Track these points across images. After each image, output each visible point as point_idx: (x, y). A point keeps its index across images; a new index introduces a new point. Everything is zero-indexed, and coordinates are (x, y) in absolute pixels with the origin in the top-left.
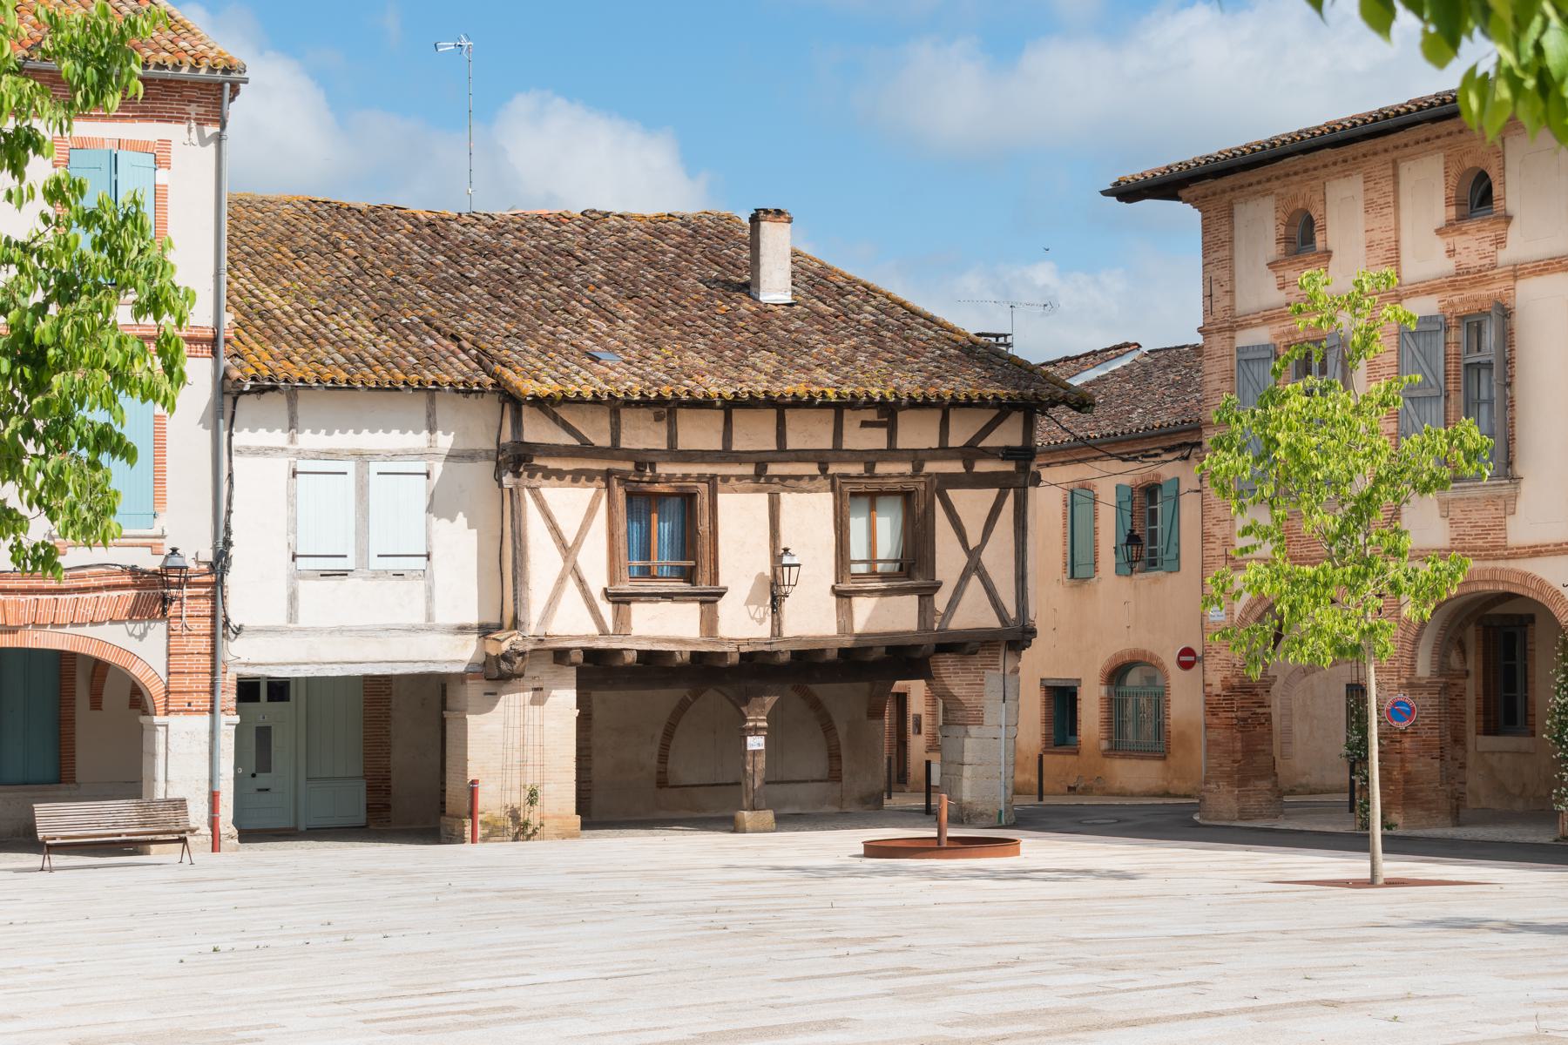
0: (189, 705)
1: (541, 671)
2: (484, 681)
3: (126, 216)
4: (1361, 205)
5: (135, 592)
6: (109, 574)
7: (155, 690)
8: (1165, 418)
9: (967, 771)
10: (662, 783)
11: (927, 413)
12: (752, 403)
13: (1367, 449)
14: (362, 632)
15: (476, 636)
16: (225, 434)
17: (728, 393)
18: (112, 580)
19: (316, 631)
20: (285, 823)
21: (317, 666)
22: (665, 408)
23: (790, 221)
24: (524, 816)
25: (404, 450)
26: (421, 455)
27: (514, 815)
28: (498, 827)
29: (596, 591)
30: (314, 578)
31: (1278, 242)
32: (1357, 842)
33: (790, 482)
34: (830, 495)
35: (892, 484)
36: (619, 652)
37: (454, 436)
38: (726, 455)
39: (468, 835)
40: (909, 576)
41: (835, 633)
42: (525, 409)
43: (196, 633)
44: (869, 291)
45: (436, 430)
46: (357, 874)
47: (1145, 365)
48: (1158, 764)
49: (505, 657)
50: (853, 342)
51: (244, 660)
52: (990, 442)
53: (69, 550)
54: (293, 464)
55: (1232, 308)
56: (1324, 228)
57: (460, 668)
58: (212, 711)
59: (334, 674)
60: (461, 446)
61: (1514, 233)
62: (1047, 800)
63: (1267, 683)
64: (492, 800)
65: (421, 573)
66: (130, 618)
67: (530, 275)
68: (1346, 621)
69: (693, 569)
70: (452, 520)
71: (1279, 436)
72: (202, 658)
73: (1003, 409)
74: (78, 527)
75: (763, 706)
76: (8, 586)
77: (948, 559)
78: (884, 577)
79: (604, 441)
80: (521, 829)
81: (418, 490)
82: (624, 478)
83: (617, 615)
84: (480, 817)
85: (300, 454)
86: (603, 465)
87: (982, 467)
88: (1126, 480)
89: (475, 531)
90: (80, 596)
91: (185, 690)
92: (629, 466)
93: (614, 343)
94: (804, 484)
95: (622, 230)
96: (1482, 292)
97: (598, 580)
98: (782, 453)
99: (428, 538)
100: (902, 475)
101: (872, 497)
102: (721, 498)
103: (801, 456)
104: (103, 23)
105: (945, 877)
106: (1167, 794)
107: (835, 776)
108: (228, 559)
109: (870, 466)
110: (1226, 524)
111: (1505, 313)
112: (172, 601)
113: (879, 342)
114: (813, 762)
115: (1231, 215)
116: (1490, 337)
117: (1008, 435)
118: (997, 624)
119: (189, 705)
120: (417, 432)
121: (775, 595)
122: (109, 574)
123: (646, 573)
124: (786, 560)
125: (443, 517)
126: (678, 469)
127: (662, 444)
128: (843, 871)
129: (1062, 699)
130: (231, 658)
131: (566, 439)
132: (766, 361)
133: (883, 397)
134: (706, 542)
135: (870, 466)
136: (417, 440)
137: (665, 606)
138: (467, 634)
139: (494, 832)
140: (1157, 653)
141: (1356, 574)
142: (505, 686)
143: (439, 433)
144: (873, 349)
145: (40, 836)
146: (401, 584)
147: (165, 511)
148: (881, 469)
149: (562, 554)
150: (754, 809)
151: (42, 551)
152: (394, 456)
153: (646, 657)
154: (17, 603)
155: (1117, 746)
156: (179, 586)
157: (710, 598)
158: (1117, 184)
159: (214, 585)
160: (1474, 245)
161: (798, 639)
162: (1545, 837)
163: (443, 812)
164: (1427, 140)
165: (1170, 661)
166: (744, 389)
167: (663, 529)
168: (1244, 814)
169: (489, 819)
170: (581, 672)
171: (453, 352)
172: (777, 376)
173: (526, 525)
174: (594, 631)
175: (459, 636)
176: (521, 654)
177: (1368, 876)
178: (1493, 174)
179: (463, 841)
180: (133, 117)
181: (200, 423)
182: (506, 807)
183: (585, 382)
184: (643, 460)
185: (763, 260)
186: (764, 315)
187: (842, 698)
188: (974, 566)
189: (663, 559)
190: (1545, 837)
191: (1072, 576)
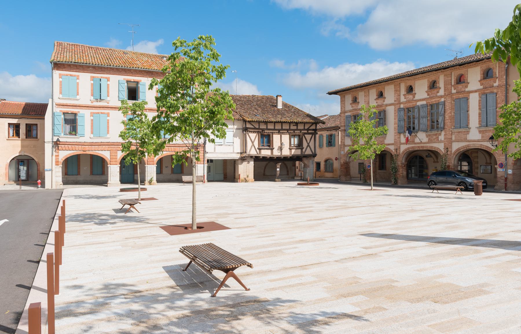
1: (248, 159)
3: (226, 94)
4: (364, 96)
8: (333, 125)
9: (307, 174)
10: (264, 175)
11: (302, 124)
12: (278, 122)
13: (371, 130)
14: (224, 153)
17: (275, 121)
20: (212, 179)
22: (266, 123)
23: (282, 97)
24: (246, 179)
26: (232, 129)
27: (245, 179)
29: (257, 148)
30: (217, 145)
31: (352, 101)
32: (370, 185)
33: (283, 133)
34: (289, 135)
35: (297, 134)
36: (260, 156)
38: (274, 129)
39: (239, 181)
40: (299, 147)
41: (289, 154)
42: (247, 122)
44: (293, 107)
46: (228, 186)
47: (329, 118)
48: (332, 173)
49: (244, 157)
50: (291, 114)
52: (311, 128)
55: (345, 110)
56: (358, 99)
57: (238, 158)
58: (204, 164)
61: (386, 100)
62: (316, 178)
63: (350, 162)
64: (242, 177)
67: (246, 104)
68: (368, 153)
69: (270, 145)
70: (237, 138)
71: (359, 128)
73: (313, 124)
74: (221, 136)
75: (279, 164)
77: (305, 144)
78: (296, 147)
79: (258, 127)
80: (246, 181)
82: (260, 133)
83: (259, 151)
84: (240, 179)
86: (257, 131)
87: (310, 132)
88: (328, 134)
92: (261, 131)
93: (258, 113)
94: (285, 134)
95: (258, 98)
96: (381, 108)
97: (257, 147)
98: (282, 129)
99: (233, 140)
100: (299, 133)
101: (294, 136)
102: (274, 135)
103: (285, 130)
104: (221, 67)
105: (311, 188)
106: (333, 178)
107: (288, 174)
108: (206, 143)
109: (294, 132)
110: (344, 140)
111: (385, 111)
112: (198, 148)
113: (295, 114)
114: (286, 173)
115: (345, 97)
116: (382, 114)
117: (313, 127)
118: (311, 154)
120: (232, 125)
121: (281, 149)
123: (263, 146)
124: (283, 144)
126: (268, 131)
127: (265, 128)
128: (293, 187)
129: (318, 164)
131: (252, 127)
132: (280, 116)
133: (296, 122)
134: (272, 141)
135: (294, 132)
137: (266, 150)
139: (242, 181)
140: (332, 158)
141: (370, 147)
144: (294, 115)
145: (183, 180)
148: (296, 132)
150: (278, 179)
151: (212, 140)
153: (263, 157)
154: (177, 148)
155: (326, 171)
156: (199, 146)
157: (272, 149)
158: (329, 92)
159: (204, 146)
160: (380, 102)
161: (284, 155)
162: (390, 184)
163: (235, 178)
164: (374, 87)
165: (334, 159)
166: (277, 120)
167: (265, 140)
168: (346, 180)
170: (254, 159)
171: (236, 114)
172: (281, 119)
174: (256, 154)
176: (246, 157)
177: (371, 189)
178: (383, 92)
179: (238, 182)
183: (255, 119)
184: (263, 130)
185: (278, 102)
186: (278, 110)
187: (289, 163)
188: (308, 146)
189: (265, 144)
190: (390, 184)
191: (320, 147)
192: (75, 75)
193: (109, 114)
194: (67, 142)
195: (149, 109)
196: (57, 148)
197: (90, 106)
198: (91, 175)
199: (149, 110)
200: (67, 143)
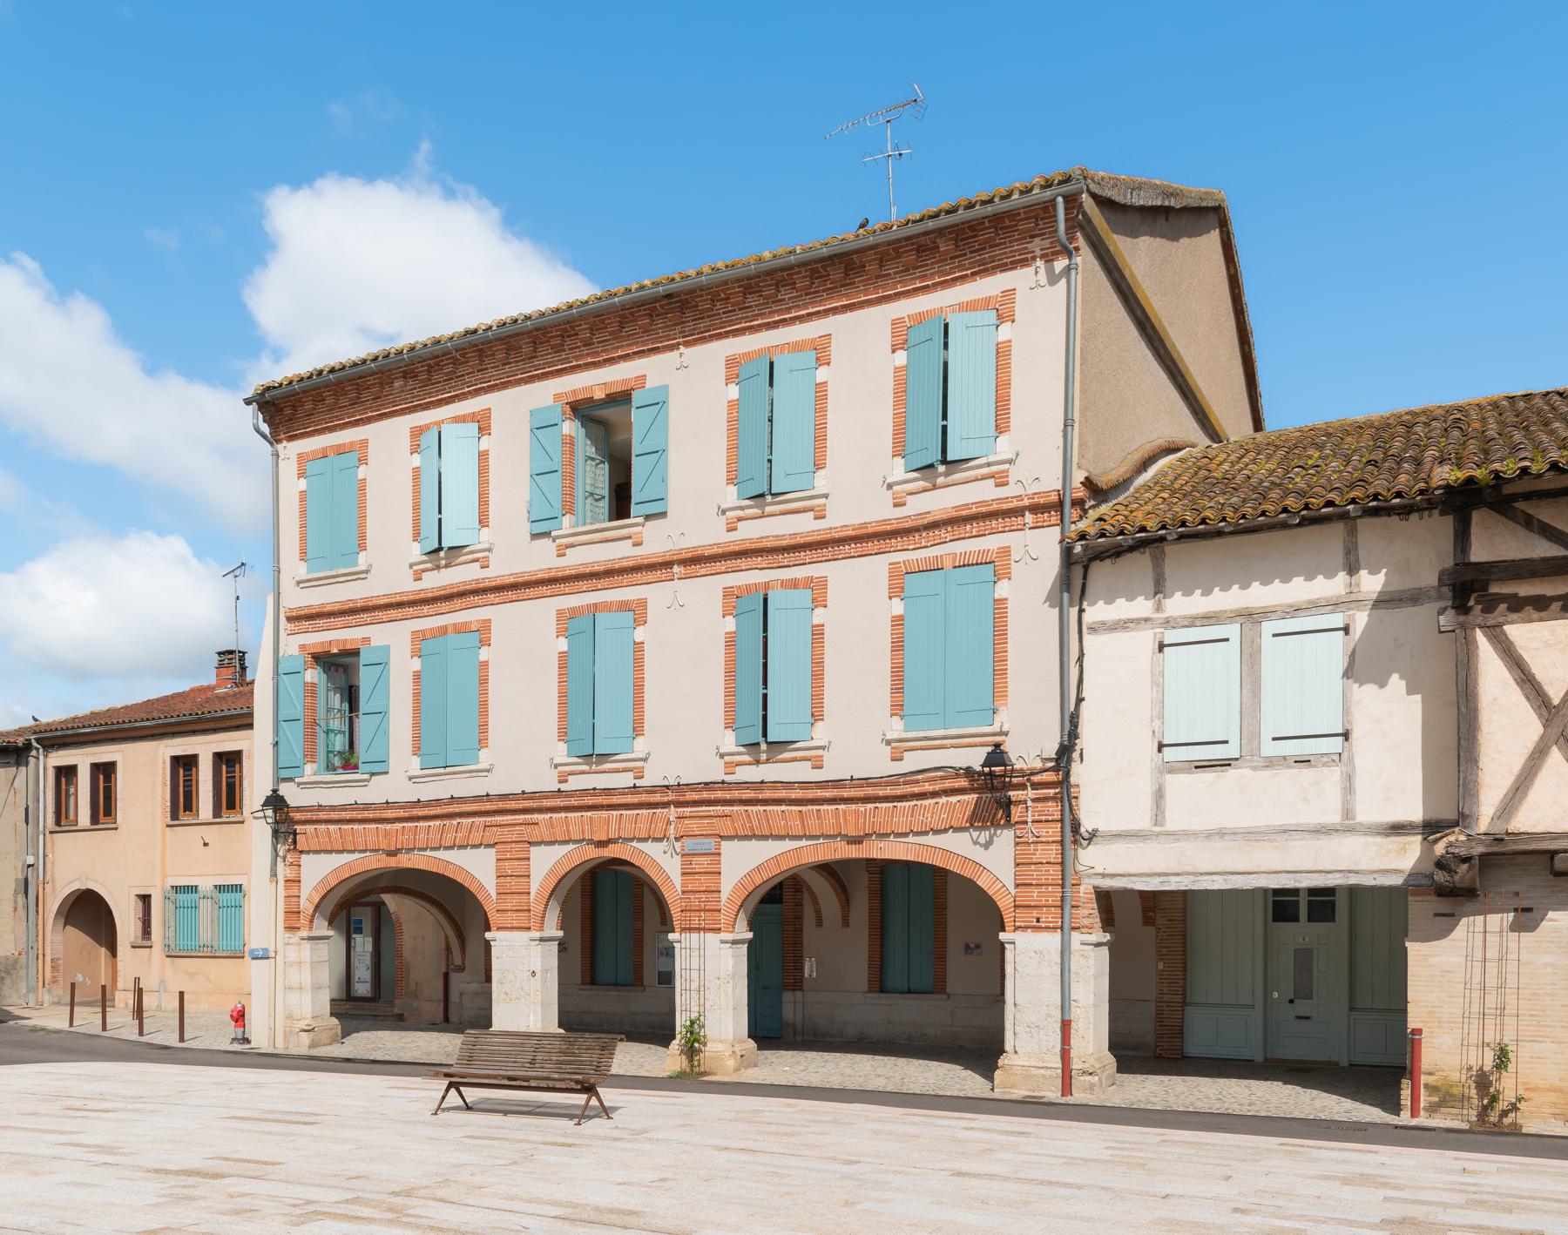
0: (1038, 921)
2: (1434, 898)
5: (976, 796)
6: (943, 778)
7: (1004, 904)
14: (1251, 835)
15: (1419, 838)
16: (1074, 611)
18: (948, 784)
19: (1187, 835)
21: (1192, 878)
25: (1310, 602)
26: (1335, 605)
28: (1451, 1095)
30: (1187, 771)
37: (1386, 574)
43: (1044, 839)
45: (1358, 570)
51: (1099, 870)
53: (906, 754)
54: (1159, 636)
57: (1397, 881)
59: (1216, 887)
60: (1397, 586)
65: (1336, 758)
66: (972, 825)
70: (1383, 684)
72: (1052, 869)
76: (846, 795)
81: (1334, 650)
84: (1424, 1079)
85: (1168, 623)
89: (1418, 697)
90: (919, 803)
91: (1032, 903)
99: (1346, 712)
119: (1038, 921)
120: (1330, 575)
122: (943, 778)
125: (1367, 682)
130: (1084, 868)
131: (1544, 549)
136: (1334, 585)
138: (1404, 834)
142: (1468, 904)
143: (1363, 573)
146: (1306, 773)
147: (1006, 704)
149: (1540, 716)
152: (1296, 610)
154: (857, 812)
169: (1439, 1084)
173: (1476, 680)
175: (1393, 838)
180: (973, 274)
181: (1045, 602)
182: (1470, 1069)
192: (352, 444)
193: (825, 586)
194: (320, 808)
195: (684, 556)
196: (290, 841)
197: (784, 543)
198: (582, 983)
199: (683, 562)
200: (322, 815)
